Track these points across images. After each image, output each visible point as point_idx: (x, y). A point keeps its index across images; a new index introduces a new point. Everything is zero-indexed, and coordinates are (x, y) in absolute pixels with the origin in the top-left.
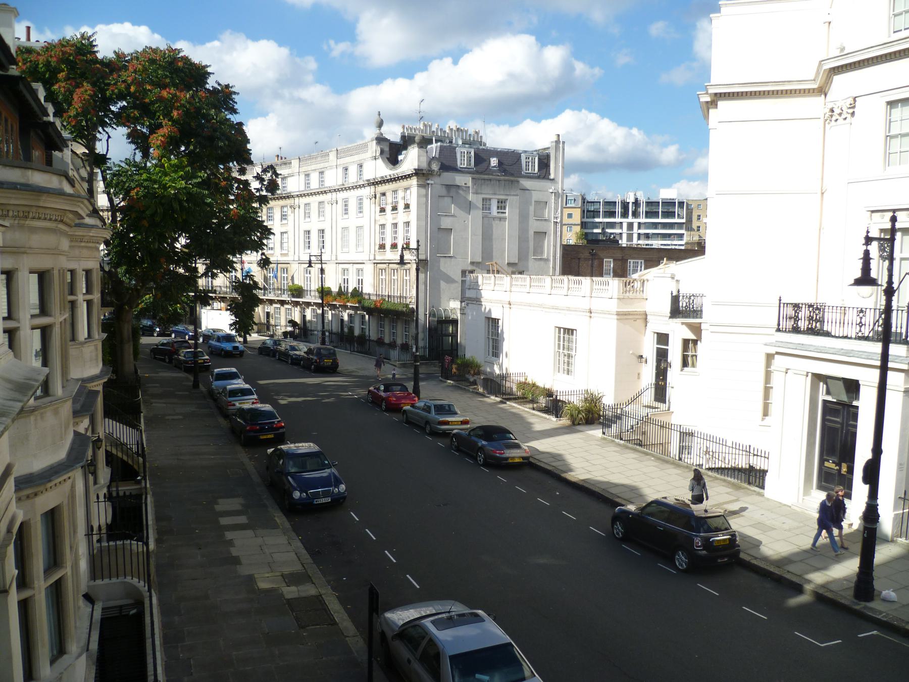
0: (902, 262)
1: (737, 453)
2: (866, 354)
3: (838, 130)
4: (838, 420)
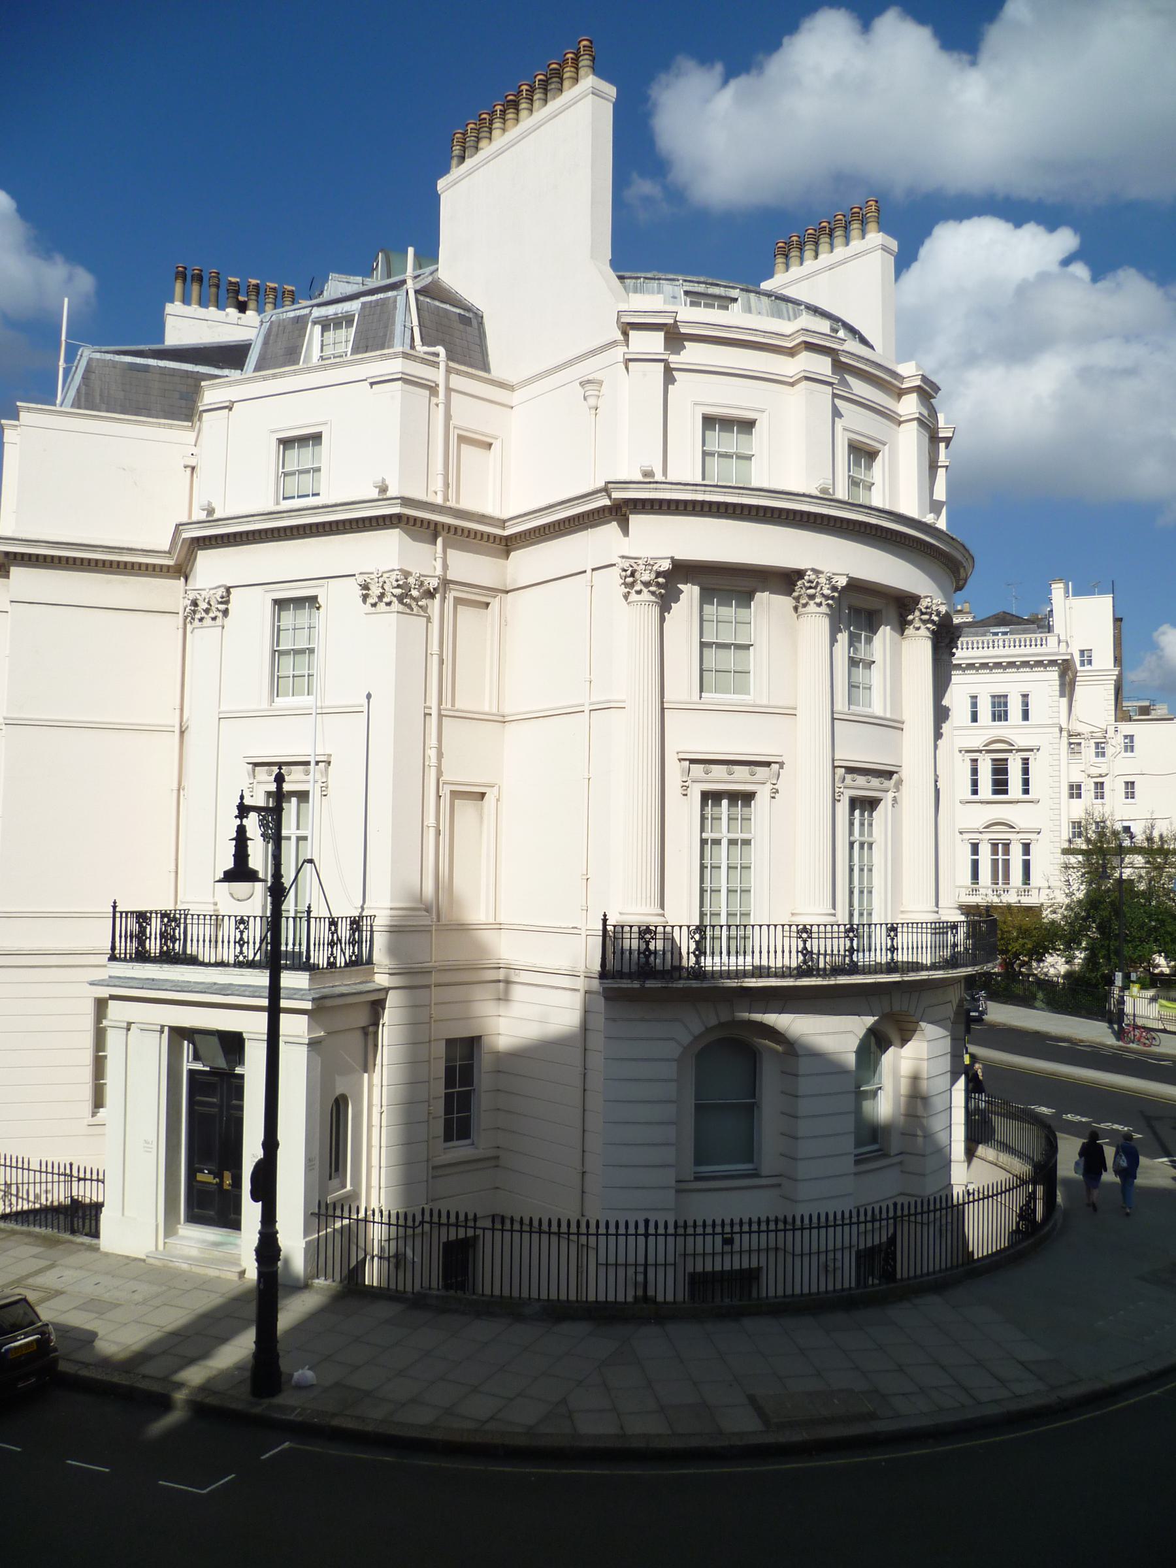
0: (301, 842)
1: (50, 1179)
2: (251, 989)
3: (204, 637)
4: (215, 1100)
